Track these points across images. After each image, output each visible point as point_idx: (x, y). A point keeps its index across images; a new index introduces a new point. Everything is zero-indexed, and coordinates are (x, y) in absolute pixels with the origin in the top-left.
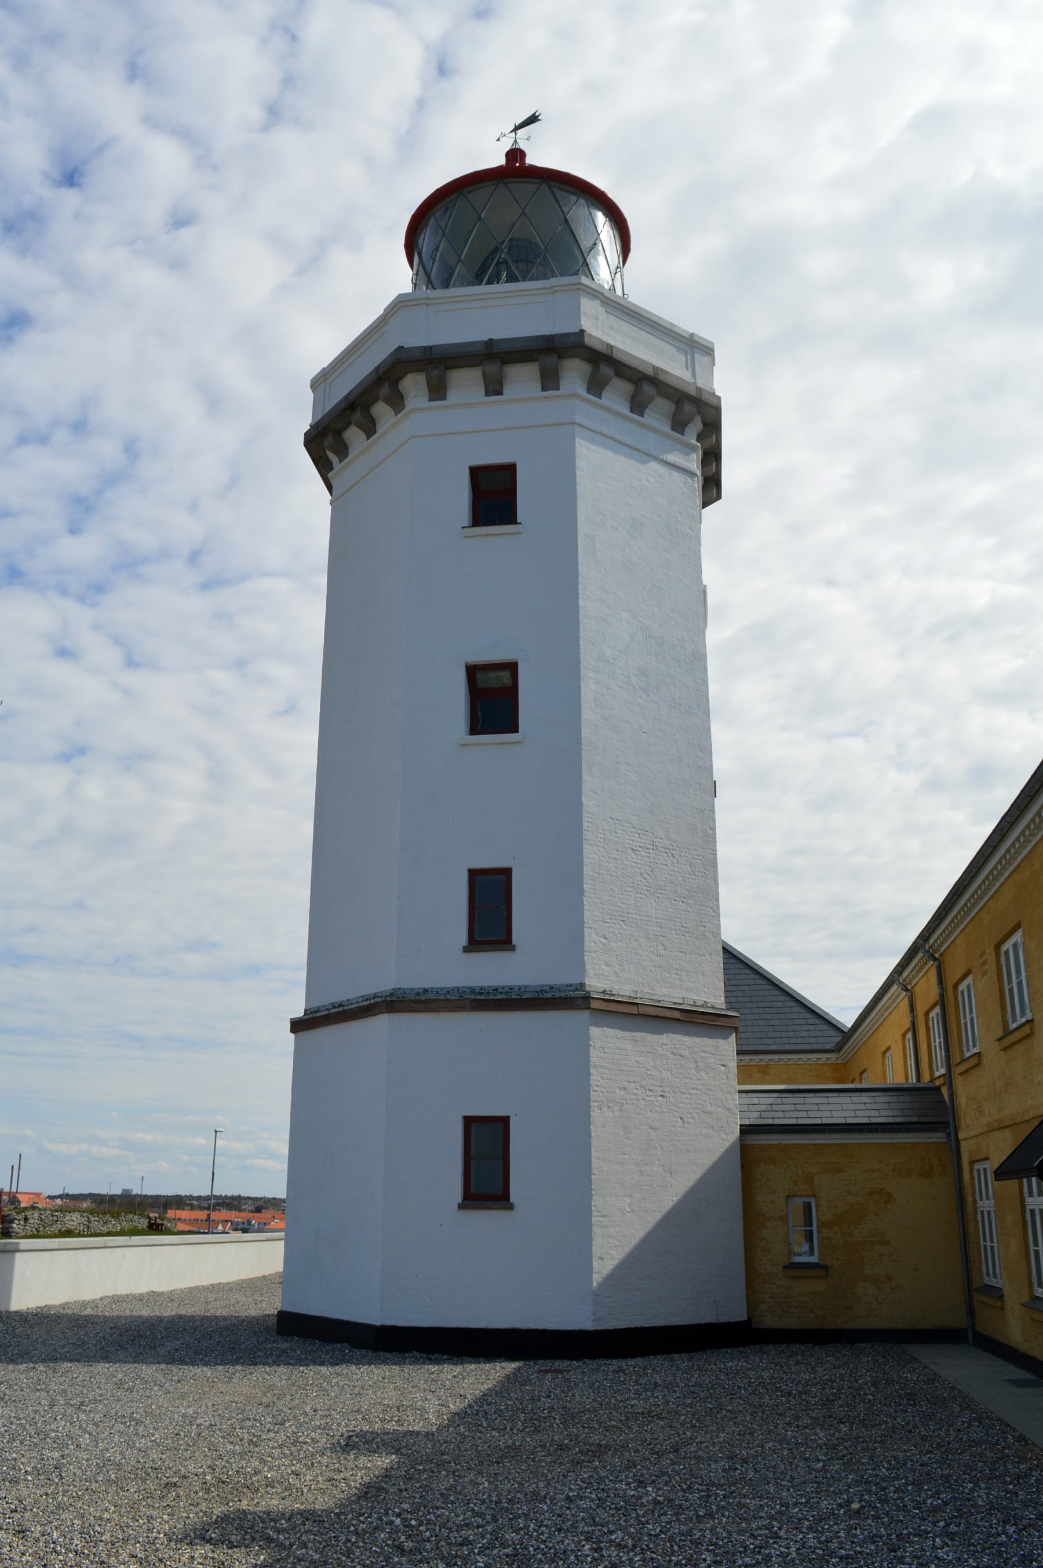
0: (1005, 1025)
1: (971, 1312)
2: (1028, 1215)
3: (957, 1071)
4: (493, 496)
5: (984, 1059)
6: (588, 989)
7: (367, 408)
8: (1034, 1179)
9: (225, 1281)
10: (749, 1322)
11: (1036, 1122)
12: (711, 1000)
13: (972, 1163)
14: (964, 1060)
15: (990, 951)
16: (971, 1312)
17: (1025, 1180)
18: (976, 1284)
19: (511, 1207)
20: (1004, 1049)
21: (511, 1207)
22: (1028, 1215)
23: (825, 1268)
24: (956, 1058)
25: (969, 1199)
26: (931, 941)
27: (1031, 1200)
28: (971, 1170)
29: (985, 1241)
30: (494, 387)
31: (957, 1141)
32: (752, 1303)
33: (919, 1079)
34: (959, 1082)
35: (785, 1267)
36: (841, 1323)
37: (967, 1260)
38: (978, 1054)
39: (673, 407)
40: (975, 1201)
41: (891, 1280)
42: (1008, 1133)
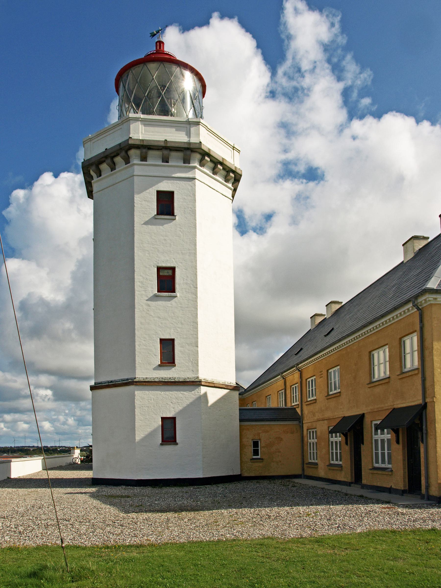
0: (328, 393)
1: (303, 470)
2: (330, 443)
3: (304, 404)
4: (166, 204)
5: (318, 401)
6: (200, 379)
7: (112, 158)
8: (338, 434)
9: (32, 473)
10: (240, 475)
11: (340, 419)
12: (232, 382)
13: (307, 430)
14: (308, 401)
15: (325, 372)
16: (303, 470)
17: (334, 434)
18: (306, 462)
19: (177, 444)
20: (327, 399)
21: (177, 444)
22: (330, 443)
23: (262, 459)
24: (304, 400)
25: (306, 439)
26: (299, 366)
27: (332, 439)
28: (307, 431)
29: (310, 450)
30: (166, 160)
31: (303, 423)
32: (241, 471)
33: (286, 405)
34: (305, 407)
35: (251, 459)
36: (267, 474)
37: (303, 456)
38: (316, 399)
39: (226, 173)
40: (308, 440)
41: (280, 462)
42: (326, 422)
